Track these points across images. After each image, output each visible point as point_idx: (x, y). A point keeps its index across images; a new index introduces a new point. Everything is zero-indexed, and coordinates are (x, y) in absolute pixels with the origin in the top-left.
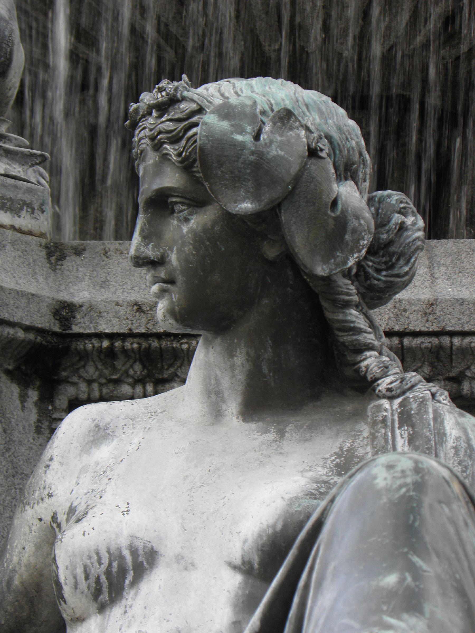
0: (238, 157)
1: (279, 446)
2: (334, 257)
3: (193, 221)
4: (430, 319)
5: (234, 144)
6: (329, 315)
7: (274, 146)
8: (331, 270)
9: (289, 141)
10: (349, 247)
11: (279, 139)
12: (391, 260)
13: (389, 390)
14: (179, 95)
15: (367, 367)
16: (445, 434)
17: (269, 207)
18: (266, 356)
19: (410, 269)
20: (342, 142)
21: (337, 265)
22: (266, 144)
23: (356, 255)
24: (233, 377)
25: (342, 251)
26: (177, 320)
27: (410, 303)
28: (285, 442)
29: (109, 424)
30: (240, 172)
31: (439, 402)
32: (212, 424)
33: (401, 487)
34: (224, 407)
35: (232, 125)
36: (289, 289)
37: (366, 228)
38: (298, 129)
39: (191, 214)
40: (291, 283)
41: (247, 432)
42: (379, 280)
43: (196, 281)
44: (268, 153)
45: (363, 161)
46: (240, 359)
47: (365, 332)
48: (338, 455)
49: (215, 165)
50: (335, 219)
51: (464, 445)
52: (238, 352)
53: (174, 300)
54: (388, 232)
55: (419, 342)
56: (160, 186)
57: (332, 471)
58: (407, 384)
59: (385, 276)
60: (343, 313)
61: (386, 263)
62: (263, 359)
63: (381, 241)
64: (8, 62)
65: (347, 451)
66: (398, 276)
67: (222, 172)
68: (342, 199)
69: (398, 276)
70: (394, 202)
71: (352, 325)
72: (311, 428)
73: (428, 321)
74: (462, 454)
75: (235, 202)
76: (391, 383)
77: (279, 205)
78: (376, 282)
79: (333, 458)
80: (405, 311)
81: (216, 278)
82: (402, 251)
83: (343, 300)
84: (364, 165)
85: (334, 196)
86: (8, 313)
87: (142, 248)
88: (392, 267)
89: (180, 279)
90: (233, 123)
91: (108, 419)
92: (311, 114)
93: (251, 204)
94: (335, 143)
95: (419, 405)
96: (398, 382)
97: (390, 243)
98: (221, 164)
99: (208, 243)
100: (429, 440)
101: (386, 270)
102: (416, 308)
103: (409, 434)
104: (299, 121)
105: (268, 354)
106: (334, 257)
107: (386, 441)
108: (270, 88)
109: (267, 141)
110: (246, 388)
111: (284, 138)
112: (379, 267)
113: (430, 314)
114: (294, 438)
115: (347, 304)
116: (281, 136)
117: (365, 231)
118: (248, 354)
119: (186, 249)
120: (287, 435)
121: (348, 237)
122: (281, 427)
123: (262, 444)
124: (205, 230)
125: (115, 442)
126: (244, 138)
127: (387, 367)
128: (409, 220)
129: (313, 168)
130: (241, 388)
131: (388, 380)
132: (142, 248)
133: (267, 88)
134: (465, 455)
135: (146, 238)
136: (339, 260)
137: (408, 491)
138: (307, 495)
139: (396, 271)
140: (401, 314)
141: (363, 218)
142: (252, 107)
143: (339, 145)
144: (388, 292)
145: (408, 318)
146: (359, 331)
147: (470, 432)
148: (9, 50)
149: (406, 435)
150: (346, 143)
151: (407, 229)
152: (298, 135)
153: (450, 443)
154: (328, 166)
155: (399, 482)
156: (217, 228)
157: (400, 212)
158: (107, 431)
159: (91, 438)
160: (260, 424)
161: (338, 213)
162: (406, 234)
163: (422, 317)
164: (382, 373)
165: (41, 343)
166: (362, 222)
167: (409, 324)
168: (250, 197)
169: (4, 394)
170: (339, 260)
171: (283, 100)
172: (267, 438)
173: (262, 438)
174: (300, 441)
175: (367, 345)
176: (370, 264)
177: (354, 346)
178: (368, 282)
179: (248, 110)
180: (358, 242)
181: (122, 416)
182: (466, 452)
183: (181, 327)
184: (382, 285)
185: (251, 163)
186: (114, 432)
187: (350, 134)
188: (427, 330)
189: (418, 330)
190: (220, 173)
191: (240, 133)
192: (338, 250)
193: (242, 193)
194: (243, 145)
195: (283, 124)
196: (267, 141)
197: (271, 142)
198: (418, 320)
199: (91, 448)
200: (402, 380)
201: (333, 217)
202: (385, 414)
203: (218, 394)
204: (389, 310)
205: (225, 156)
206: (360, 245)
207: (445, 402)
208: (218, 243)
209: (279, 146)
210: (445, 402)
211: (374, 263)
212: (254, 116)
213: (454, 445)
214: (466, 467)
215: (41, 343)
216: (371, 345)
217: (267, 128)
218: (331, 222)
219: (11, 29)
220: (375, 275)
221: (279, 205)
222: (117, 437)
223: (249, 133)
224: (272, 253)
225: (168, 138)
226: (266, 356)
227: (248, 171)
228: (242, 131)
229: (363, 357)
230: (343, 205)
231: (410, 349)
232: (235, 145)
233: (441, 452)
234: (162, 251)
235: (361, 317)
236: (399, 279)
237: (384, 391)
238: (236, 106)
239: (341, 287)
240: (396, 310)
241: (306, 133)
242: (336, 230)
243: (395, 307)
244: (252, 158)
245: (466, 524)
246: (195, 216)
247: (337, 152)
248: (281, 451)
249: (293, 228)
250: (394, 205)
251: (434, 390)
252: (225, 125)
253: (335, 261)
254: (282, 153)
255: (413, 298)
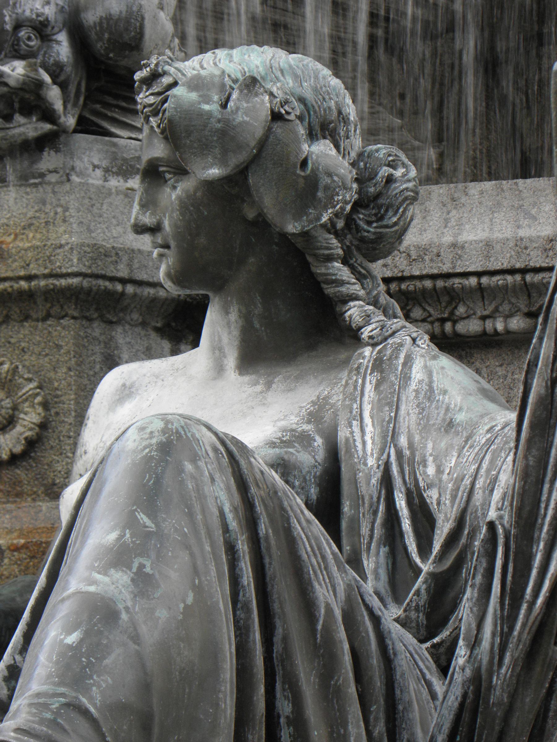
0: (205, 126)
1: (264, 397)
2: (307, 214)
3: (179, 188)
4: (550, 255)
5: (201, 114)
6: (313, 269)
7: (240, 113)
8: (303, 227)
9: (254, 107)
10: (323, 203)
11: (245, 105)
12: (379, 212)
13: (371, 337)
14: (160, 70)
15: (350, 317)
16: (410, 378)
17: (235, 171)
18: (256, 312)
19: (399, 219)
20: (317, 103)
21: (310, 222)
22: (232, 111)
23: (330, 211)
24: (230, 333)
25: (315, 208)
26: (174, 283)
27: (531, 240)
28: (270, 393)
29: (134, 382)
30: (207, 140)
31: (418, 346)
32: (215, 379)
33: (145, 448)
34: (226, 362)
35: (200, 96)
36: (274, 246)
37: (340, 184)
38: (262, 95)
39: (177, 181)
40: (276, 240)
41: (239, 386)
42: (368, 232)
43: (185, 245)
44: (234, 120)
45: (343, 119)
46: (233, 316)
47: (348, 283)
48: (314, 403)
49: (183, 135)
50: (305, 178)
51: (425, 387)
52: (232, 310)
53: (170, 263)
54: (375, 186)
55: (540, 278)
56: (150, 157)
57: (304, 419)
58: (387, 331)
59: (375, 227)
60: (325, 266)
61: (376, 215)
62: (253, 315)
63: (369, 194)
64: (139, 36)
65: (323, 399)
66: (387, 227)
67: (191, 141)
68: (312, 158)
69: (387, 227)
70: (381, 156)
71: (334, 278)
72: (298, 378)
73: (547, 256)
74: (421, 396)
75: (203, 169)
76: (372, 331)
77: (246, 168)
78: (366, 234)
79: (309, 406)
80: (526, 248)
81: (202, 240)
82: (389, 203)
83: (323, 255)
84: (345, 122)
85: (304, 156)
86: (147, 274)
87: (140, 216)
88: (381, 218)
89: (173, 244)
90: (201, 93)
91: (134, 378)
92: (285, 79)
93: (219, 169)
94: (309, 105)
95: (393, 351)
96: (378, 329)
97: (378, 195)
98: (189, 134)
99: (192, 208)
100: (394, 385)
101: (377, 221)
102: (537, 245)
103: (377, 380)
104: (263, 87)
105: (259, 309)
106: (307, 214)
107: (355, 387)
108: (249, 56)
109: (234, 108)
110: (241, 343)
111: (250, 105)
112: (370, 219)
113: (550, 249)
114: (279, 389)
115: (330, 258)
116: (248, 102)
117: (339, 187)
118: (240, 311)
119: (175, 215)
120: (274, 386)
121: (320, 194)
122: (270, 379)
123: (250, 395)
124: (188, 197)
125: (137, 399)
126: (211, 107)
127: (369, 316)
128: (399, 173)
129: (279, 131)
130: (236, 343)
131: (369, 328)
132: (140, 216)
133: (246, 56)
134: (425, 397)
135: (144, 206)
136: (311, 217)
137: (150, 452)
138: (267, 444)
139: (385, 222)
140: (522, 252)
141: (337, 175)
142: (220, 76)
143: (313, 107)
144: (381, 243)
145: (529, 255)
146: (342, 283)
147: (435, 374)
148: (138, 24)
149: (374, 382)
150: (322, 103)
151: (395, 181)
152: (263, 101)
153: (413, 386)
154: (296, 127)
155: (144, 443)
156: (199, 194)
157: (389, 165)
158: (132, 390)
159: (117, 397)
160: (253, 377)
161: (308, 172)
162: (394, 185)
163: (542, 254)
164: (364, 322)
165: (186, 300)
166: (336, 178)
167: (529, 260)
168: (217, 163)
169: (153, 350)
170: (311, 217)
171: (257, 67)
172: (255, 390)
173: (250, 390)
174: (284, 391)
175: (351, 296)
176: (361, 216)
177: (338, 297)
178: (359, 234)
179: (216, 80)
180: (332, 198)
181: (148, 375)
182: (426, 394)
183: (179, 288)
184: (372, 237)
185: (217, 130)
186: (137, 390)
187: (329, 94)
188: (546, 265)
189: (538, 266)
190: (188, 142)
191: (207, 103)
192: (310, 207)
193: (210, 160)
194: (209, 114)
195: (250, 91)
196: (234, 108)
197: (238, 109)
198: (538, 256)
199: (116, 406)
200: (382, 327)
201: (303, 177)
202: (362, 361)
203: (221, 349)
204: (510, 248)
205: (193, 126)
206: (334, 201)
207: (423, 346)
208: (201, 208)
209: (245, 113)
210: (423, 346)
211: (365, 216)
212: (223, 85)
213: (416, 388)
214: (423, 409)
215: (186, 300)
216: (354, 296)
217: (235, 96)
218: (301, 181)
219: (140, 4)
220: (366, 227)
221: (246, 168)
222: (140, 394)
223: (216, 102)
224: (251, 214)
225: (151, 112)
226: (256, 312)
227: (215, 138)
228: (208, 101)
229: (347, 308)
230: (313, 164)
231: (533, 285)
232: (202, 115)
233: (404, 395)
234: (158, 217)
235: (346, 269)
236: (388, 230)
237: (367, 339)
238: (205, 76)
239: (320, 242)
240: (517, 248)
241: (269, 98)
242: (309, 188)
243: (516, 245)
244: (219, 126)
245: (213, 480)
246: (180, 184)
247: (312, 113)
248: (265, 402)
249: (262, 190)
250: (381, 159)
251: (414, 335)
252: (194, 96)
253: (307, 217)
254: (248, 119)
255: (533, 235)
